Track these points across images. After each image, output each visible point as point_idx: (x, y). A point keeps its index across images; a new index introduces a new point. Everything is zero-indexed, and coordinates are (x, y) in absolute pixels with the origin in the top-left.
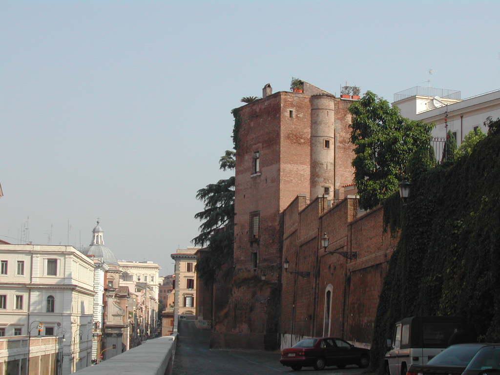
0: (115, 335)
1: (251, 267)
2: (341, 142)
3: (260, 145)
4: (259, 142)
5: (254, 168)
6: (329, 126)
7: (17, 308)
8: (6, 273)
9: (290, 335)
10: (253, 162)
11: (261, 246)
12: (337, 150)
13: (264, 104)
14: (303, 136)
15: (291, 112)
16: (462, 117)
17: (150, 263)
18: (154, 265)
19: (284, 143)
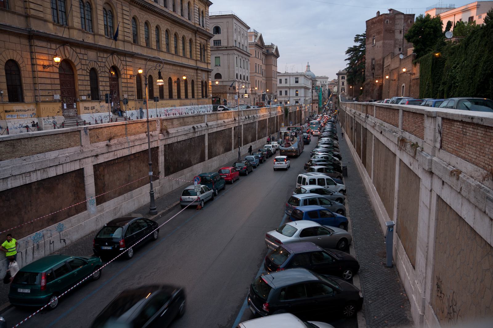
2: (406, 31)
9: (60, 89)
15: (387, 21)
16: (455, 15)
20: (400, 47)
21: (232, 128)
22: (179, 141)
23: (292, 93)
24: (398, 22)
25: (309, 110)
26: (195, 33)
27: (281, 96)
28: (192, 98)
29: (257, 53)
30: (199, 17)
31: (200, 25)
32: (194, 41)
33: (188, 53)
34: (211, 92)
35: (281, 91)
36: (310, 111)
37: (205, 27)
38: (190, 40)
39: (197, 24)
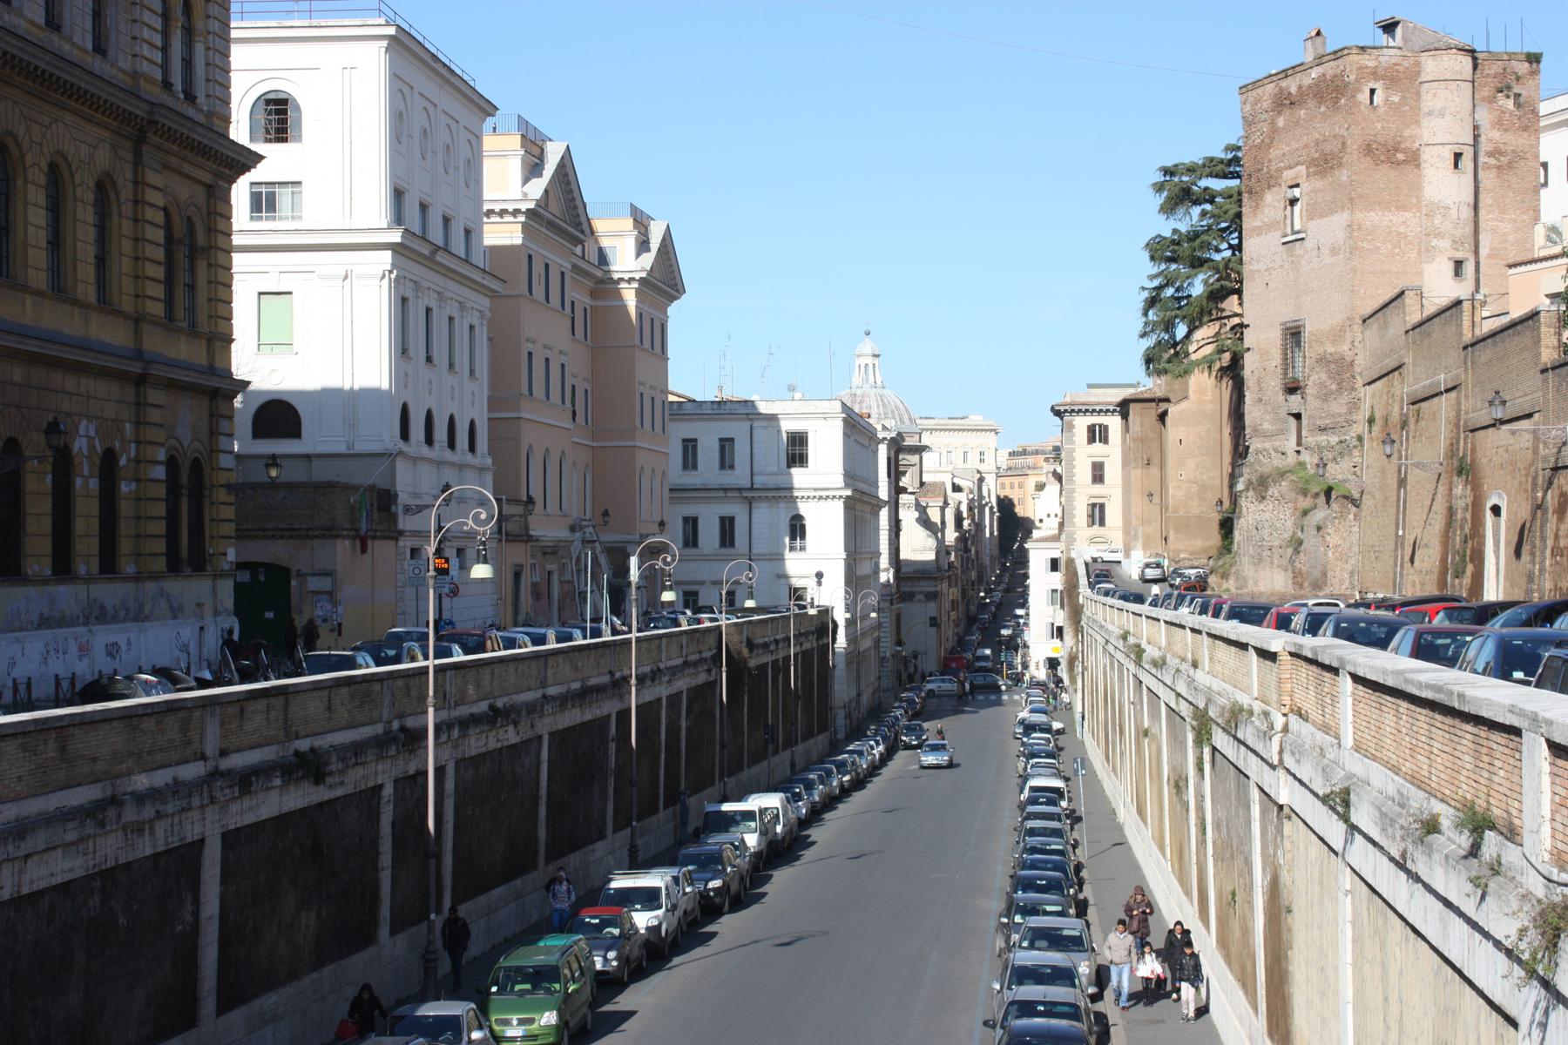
0: (921, 597)
2: (1490, 154)
3: (1302, 169)
8: (695, 467)
11: (1309, 398)
12: (1481, 174)
13: (1311, 73)
15: (1372, 91)
17: (976, 419)
18: (987, 423)
20: (1459, 255)
21: (381, 787)
22: (25, 890)
24: (1433, 98)
25: (878, 641)
26: (139, 141)
28: (102, 571)
30: (166, 34)
31: (167, 85)
32: (126, 191)
33: (87, 272)
34: (228, 529)
35: (695, 520)
36: (888, 648)
37: (201, 98)
38: (100, 186)
39: (149, 80)
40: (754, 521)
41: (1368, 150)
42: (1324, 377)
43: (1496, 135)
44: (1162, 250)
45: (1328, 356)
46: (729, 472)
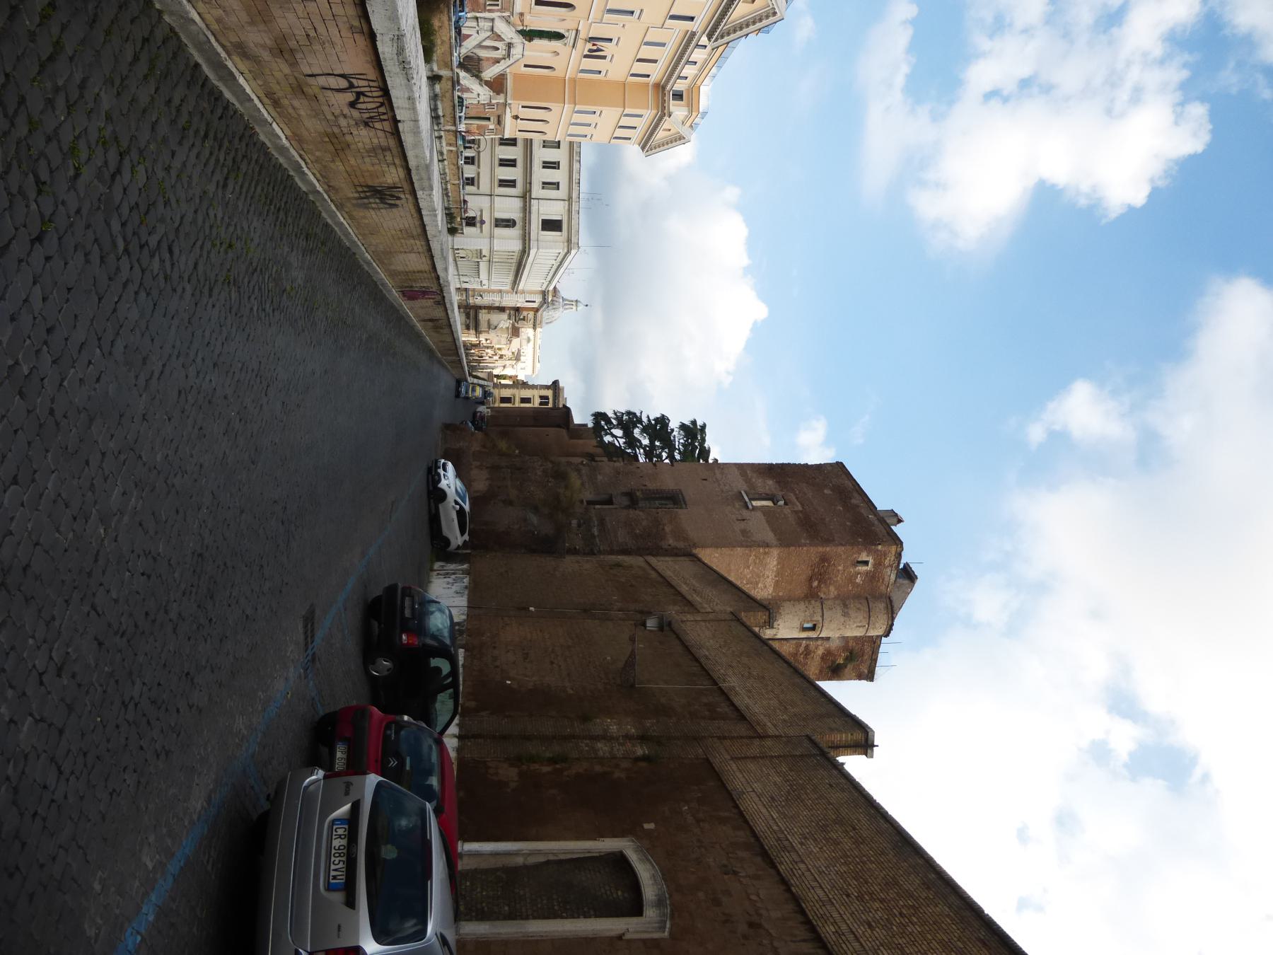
1: (588, 495)
2: (807, 647)
4: (803, 505)
5: (757, 496)
6: (839, 629)
7: (501, 160)
8: (544, 167)
10: (767, 494)
12: (794, 642)
14: (822, 586)
15: (866, 563)
17: (538, 365)
19: (812, 552)
23: (508, 206)
27: (497, 162)
29: (513, 254)
35: (514, 166)
40: (513, 198)
41: (824, 559)
42: (644, 523)
43: (820, 651)
44: (663, 421)
45: (661, 527)
46: (541, 187)
